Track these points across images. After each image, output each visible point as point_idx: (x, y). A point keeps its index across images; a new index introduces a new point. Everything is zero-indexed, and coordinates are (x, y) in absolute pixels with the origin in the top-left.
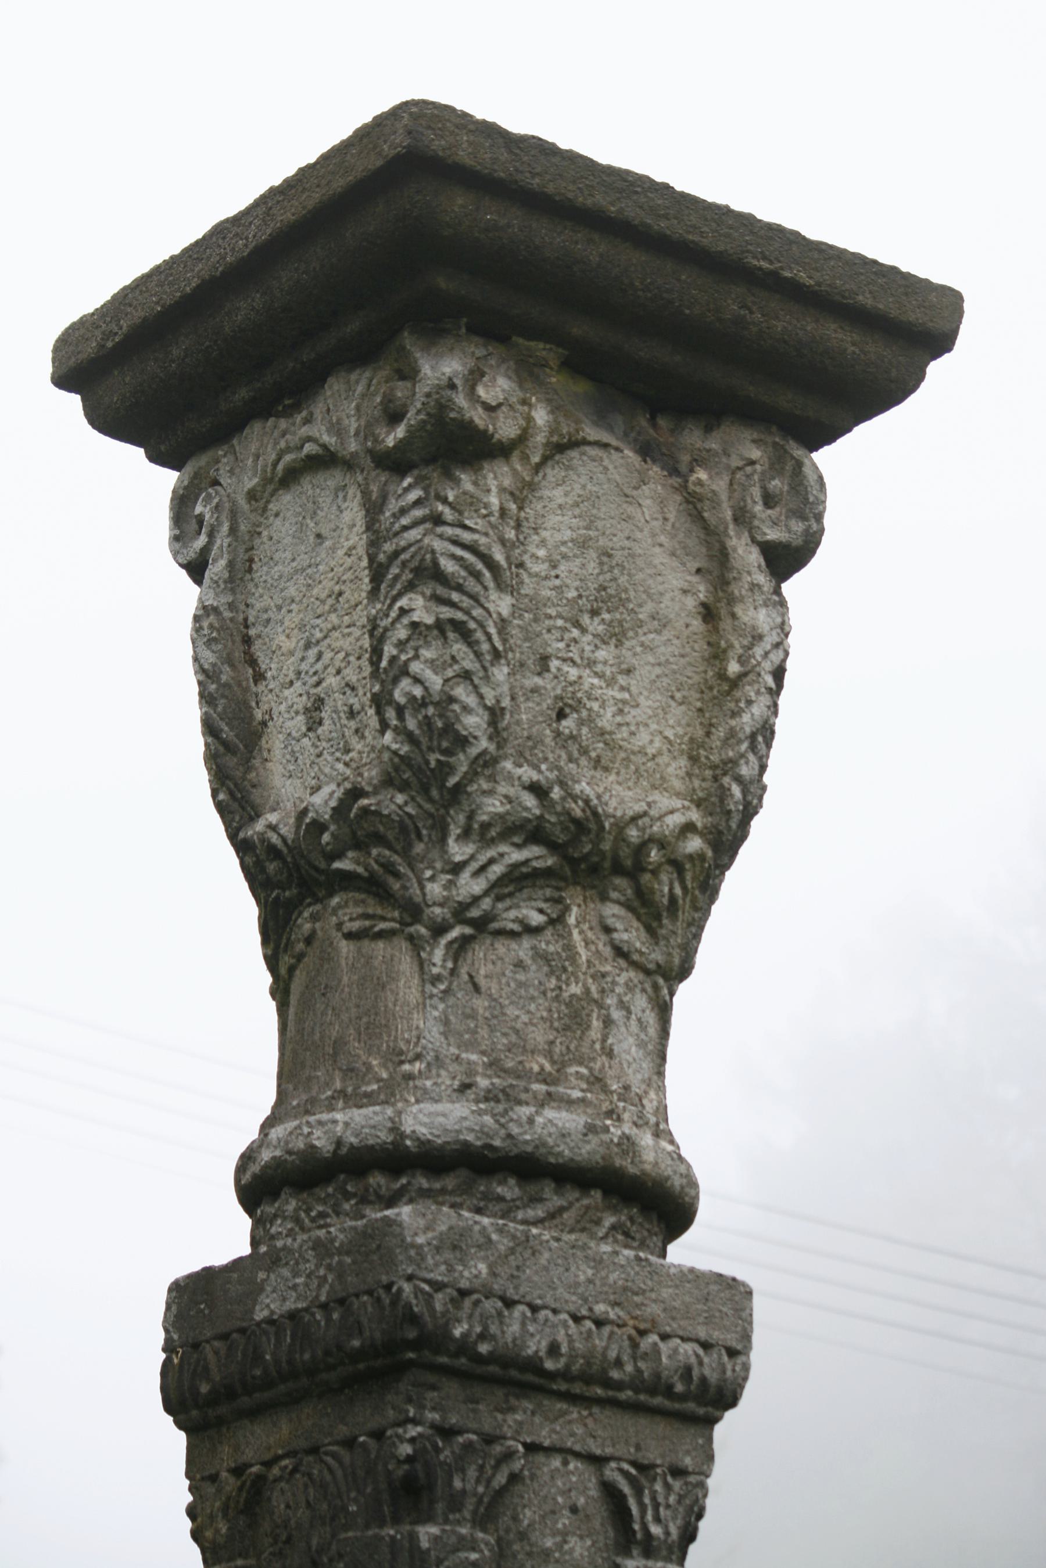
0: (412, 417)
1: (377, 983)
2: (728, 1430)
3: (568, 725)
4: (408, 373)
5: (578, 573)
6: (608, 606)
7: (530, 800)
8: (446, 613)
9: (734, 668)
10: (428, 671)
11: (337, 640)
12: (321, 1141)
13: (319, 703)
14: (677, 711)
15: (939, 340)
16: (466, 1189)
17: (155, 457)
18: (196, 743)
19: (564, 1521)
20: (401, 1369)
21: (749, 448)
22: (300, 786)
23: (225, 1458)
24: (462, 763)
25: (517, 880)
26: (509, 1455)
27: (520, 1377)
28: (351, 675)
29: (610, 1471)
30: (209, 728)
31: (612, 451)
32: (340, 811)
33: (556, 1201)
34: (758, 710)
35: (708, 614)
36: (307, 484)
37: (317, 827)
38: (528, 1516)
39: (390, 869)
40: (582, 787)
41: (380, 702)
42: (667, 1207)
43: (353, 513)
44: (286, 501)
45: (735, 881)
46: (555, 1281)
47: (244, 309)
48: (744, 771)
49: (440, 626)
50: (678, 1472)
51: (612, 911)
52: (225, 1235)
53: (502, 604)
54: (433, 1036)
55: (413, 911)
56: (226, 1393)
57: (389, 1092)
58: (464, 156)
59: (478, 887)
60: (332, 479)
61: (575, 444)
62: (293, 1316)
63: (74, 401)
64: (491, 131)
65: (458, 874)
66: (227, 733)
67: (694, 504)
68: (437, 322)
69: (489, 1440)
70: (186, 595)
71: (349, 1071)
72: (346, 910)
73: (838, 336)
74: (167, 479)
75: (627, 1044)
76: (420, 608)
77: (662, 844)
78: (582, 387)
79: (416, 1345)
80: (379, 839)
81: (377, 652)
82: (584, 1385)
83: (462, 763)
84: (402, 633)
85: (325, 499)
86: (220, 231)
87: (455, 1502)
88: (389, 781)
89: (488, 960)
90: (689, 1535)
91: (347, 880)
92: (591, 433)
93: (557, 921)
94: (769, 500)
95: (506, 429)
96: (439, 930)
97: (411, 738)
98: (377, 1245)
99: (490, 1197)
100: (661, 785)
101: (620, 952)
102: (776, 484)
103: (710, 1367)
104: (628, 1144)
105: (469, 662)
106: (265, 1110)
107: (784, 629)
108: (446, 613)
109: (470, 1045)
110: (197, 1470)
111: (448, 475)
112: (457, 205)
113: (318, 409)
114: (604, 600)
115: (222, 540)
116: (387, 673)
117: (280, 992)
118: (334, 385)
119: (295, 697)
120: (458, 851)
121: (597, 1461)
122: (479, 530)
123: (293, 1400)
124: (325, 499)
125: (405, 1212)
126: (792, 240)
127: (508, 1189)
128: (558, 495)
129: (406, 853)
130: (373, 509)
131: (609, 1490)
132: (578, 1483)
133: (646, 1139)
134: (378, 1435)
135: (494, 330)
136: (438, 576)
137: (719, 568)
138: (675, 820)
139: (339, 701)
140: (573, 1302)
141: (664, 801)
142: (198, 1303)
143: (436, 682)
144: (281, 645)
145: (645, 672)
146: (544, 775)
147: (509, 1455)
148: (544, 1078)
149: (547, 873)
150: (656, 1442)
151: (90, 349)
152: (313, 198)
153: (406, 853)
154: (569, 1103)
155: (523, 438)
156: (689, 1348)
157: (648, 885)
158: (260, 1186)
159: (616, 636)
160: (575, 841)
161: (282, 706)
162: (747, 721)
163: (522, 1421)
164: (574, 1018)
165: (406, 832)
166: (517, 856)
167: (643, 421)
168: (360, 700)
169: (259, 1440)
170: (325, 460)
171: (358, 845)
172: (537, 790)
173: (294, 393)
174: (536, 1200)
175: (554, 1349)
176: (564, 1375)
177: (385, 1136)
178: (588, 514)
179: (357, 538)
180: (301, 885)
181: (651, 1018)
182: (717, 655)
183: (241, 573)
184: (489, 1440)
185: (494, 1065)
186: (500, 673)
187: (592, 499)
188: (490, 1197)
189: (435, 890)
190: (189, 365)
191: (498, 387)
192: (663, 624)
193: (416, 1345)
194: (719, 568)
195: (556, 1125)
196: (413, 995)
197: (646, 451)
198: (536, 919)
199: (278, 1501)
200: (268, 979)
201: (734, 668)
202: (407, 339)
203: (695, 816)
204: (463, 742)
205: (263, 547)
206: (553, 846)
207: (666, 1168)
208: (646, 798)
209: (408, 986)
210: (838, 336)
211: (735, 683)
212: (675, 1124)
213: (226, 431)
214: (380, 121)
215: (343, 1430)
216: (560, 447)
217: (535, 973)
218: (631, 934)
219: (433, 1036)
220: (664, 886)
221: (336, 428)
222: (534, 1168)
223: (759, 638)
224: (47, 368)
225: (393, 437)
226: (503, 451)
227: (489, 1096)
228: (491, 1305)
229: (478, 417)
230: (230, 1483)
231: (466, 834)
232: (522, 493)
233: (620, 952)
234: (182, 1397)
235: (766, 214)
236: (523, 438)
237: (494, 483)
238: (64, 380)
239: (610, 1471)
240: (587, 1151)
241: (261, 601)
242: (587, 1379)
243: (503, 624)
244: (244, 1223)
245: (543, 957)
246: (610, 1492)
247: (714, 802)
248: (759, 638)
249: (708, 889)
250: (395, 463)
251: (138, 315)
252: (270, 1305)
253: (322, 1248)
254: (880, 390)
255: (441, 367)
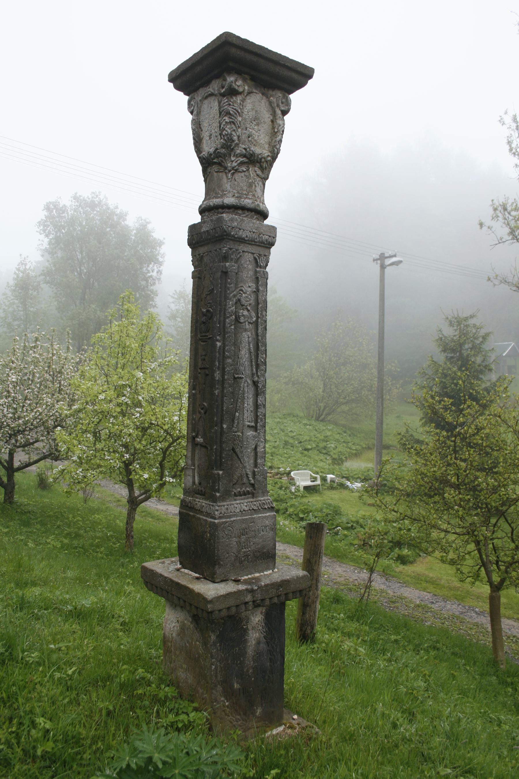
0: (226, 87)
1: (220, 180)
2: (273, 249)
3: (250, 139)
4: (225, 80)
5: (252, 114)
6: (257, 120)
7: (244, 151)
8: (231, 120)
9: (276, 130)
10: (228, 130)
11: (214, 124)
12: (211, 204)
13: (211, 135)
14: (267, 137)
15: (310, 77)
16: (234, 212)
17: (185, 94)
18: (192, 141)
19: (248, 263)
20: (224, 239)
21: (279, 94)
22: (208, 148)
23: (197, 253)
24: (233, 145)
25: (242, 163)
26: (240, 253)
27: (242, 241)
28: (216, 130)
29: (255, 255)
30: (194, 139)
31: (245, 754)
32: (214, 152)
33: (247, 214)
34: (280, 137)
35: (272, 121)
36: (209, 99)
37: (211, 155)
38: (242, 262)
39: (222, 161)
40: (252, 149)
41: (220, 134)
42: (264, 215)
43: (216, 103)
44: (206, 102)
45: (275, 165)
46: (247, 226)
47: (199, 69)
48: (277, 147)
49: (230, 122)
50: (265, 256)
51: (256, 169)
52: (197, 219)
53: (240, 119)
54: (229, 188)
55: (226, 168)
56: (197, 243)
57: (222, 197)
58: (234, 42)
59: (236, 164)
60: (213, 98)
61: (252, 92)
62: (207, 231)
63: (172, 84)
64: (239, 38)
65: (233, 162)
66: (197, 139)
67: (270, 103)
68: (230, 71)
69: (237, 250)
70: (190, 117)
71: (216, 193)
72: (215, 168)
73: (294, 75)
74: (187, 98)
75: (258, 190)
76: (227, 119)
77: (264, 158)
78: (253, 83)
79: (226, 235)
80: (220, 157)
81: (220, 126)
82: (251, 242)
83: (233, 145)
84: (224, 123)
85: (212, 101)
86: (195, 55)
87: (232, 260)
88: (222, 147)
89: (237, 176)
90: (267, 265)
91: (215, 163)
92: (254, 91)
93: (248, 170)
94: (282, 103)
95: (241, 90)
96: (230, 171)
97: (225, 140)
98: (220, 220)
99: (237, 213)
100: (264, 149)
101: (258, 175)
102: (283, 100)
103: (270, 240)
104: (258, 205)
105: (235, 128)
106: (203, 199)
107: (284, 124)
108: (231, 120)
109: (234, 189)
110: (193, 255)
111: (231, 97)
112: (233, 51)
113: (211, 86)
114: (256, 119)
115: (196, 108)
116: (222, 130)
117: (205, 181)
118: (213, 82)
119: (207, 134)
120: (233, 159)
121: (253, 254)
122: (236, 106)
123: (208, 244)
124: (212, 101)
125: (224, 215)
126: (287, 58)
127: (240, 212)
128: (249, 101)
129: (225, 159)
130: (219, 103)
131: (255, 258)
132: (250, 257)
133: (261, 204)
134: (220, 249)
135: (239, 73)
136: (230, 114)
137: (274, 114)
138: (266, 155)
139: (214, 134)
140: (250, 229)
141: (265, 151)
142: (193, 229)
143: (229, 131)
144: (205, 125)
145: (262, 131)
146: (246, 147)
147: (240, 253)
148: (246, 195)
149: (246, 162)
150: (262, 251)
151: (174, 75)
152: (210, 49)
153: (225, 159)
154: (249, 199)
155: (243, 91)
156: (267, 237)
157: (261, 165)
158: (202, 211)
159: (258, 124)
160: (251, 157)
161: (205, 135)
162: (278, 139)
163: (242, 247)
164: (250, 185)
165: (225, 155)
166: (242, 160)
167: (263, 89)
168: (218, 134)
169: (202, 250)
170: (212, 95)
171: (217, 157)
172: (245, 149)
173: (207, 83)
174: (244, 213)
175: (247, 236)
176: (248, 240)
177: (221, 203)
178: (254, 104)
179: (217, 108)
180: (209, 164)
181: (262, 186)
182: (273, 128)
183: (199, 114)
184: (237, 250)
185: (238, 192)
186: (239, 130)
187: (254, 102)
188: (237, 213)
189: (229, 165)
190: (190, 78)
191: (239, 83)
192: (265, 123)
193: (226, 235)
194: (274, 114)
195: (247, 202)
196: (226, 181)
197: (263, 94)
198: (245, 170)
199: (205, 259)
200: (203, 179)
201: (276, 130)
202: (225, 74)
203: (269, 154)
204: (233, 141)
205: (202, 109)
206: (247, 158)
207: (264, 209)
208: (262, 150)
209: (225, 180)
210: (294, 75)
211: (276, 133)
212: (265, 202)
213: (196, 90)
214: (221, 35)
215: (215, 248)
216: (249, 93)
217: (244, 178)
218: (259, 172)
219: (229, 188)
220: (265, 165)
221: (214, 89)
222: (244, 208)
223: (280, 125)
224: (167, 78)
225: (223, 91)
226: (240, 93)
227: (237, 197)
228: (237, 230)
229: (236, 88)
230: (198, 256)
231: (234, 156)
232: (243, 100)
233: (258, 175)
234: (191, 243)
235: (283, 54)
236: (243, 91)
237: (239, 99)
238: (170, 80)
239: (255, 255)
240: (252, 206)
241: (202, 118)
242: (252, 241)
243: (240, 122)
244: (200, 217)
245: (245, 175)
246: (255, 259)
247: (272, 152)
248: (280, 125)
249: (271, 165)
250: (223, 95)
251: (181, 70)
252: (204, 229)
253: (212, 221)
254: (299, 84)
255: (231, 79)
